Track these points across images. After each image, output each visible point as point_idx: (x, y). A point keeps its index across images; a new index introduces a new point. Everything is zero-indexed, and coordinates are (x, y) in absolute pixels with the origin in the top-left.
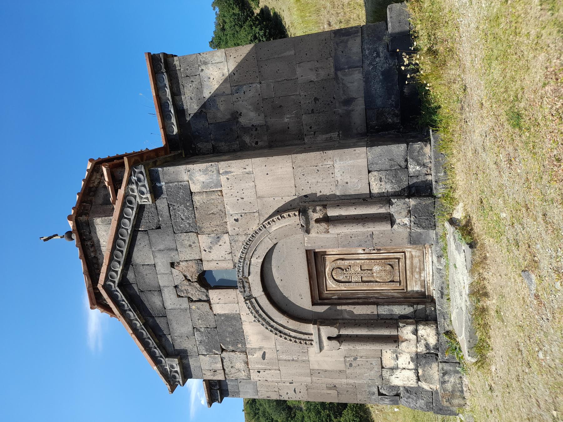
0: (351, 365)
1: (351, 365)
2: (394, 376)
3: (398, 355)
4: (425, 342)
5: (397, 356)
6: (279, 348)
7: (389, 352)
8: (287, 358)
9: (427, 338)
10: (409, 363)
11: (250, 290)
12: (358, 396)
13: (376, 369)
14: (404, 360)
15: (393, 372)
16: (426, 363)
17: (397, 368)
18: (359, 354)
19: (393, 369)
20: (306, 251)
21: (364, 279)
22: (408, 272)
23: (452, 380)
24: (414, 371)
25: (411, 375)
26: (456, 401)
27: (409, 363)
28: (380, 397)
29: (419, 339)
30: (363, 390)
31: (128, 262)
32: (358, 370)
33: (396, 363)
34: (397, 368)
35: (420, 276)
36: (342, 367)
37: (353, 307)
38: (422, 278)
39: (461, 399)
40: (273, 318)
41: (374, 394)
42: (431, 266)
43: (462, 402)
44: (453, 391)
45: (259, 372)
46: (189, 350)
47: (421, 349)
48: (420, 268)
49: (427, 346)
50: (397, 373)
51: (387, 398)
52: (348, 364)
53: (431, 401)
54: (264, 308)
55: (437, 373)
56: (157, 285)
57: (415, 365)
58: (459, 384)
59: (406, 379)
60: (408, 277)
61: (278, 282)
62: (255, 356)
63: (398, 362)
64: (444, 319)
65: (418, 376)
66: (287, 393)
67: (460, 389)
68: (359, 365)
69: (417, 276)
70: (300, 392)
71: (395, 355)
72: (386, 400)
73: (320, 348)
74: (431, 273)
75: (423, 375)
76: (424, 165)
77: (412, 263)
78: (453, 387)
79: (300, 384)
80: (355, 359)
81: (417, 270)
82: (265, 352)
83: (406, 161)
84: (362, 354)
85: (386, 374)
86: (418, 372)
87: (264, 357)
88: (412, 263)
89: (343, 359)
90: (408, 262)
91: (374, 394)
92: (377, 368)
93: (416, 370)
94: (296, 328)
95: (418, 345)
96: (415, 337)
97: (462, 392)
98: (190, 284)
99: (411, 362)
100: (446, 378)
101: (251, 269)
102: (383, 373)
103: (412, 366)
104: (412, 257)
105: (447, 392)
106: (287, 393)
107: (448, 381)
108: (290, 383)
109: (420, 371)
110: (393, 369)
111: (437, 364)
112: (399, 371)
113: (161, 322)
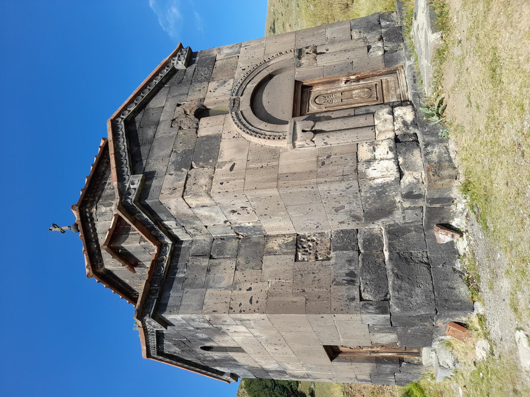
0: (323, 164)
1: (323, 164)
2: (370, 169)
3: (376, 147)
4: (402, 120)
5: (374, 148)
6: (250, 158)
7: (365, 145)
8: (257, 166)
9: (404, 117)
10: (388, 152)
11: (239, 106)
12: (333, 303)
13: (351, 164)
14: (383, 150)
15: (370, 165)
16: (406, 150)
17: (375, 159)
18: (333, 152)
19: (369, 162)
20: (296, 81)
21: (359, 377)
22: (384, 91)
23: (436, 149)
24: (393, 160)
25: (392, 165)
26: (445, 173)
27: (388, 152)
28: (362, 303)
29: (395, 119)
30: (340, 294)
31: (142, 107)
32: (331, 168)
33: (373, 155)
34: (375, 159)
35: (396, 92)
36: (313, 167)
37: (331, 113)
38: (398, 93)
39: (451, 169)
40: (253, 124)
41: (353, 299)
42: (404, 80)
43: (453, 173)
44: (440, 162)
45: (222, 184)
46: (158, 171)
47: (398, 126)
48: (395, 88)
49: (405, 123)
50: (375, 165)
51: (371, 305)
52: (320, 163)
53: (431, 289)
54: (247, 118)
55: (420, 158)
56: (157, 120)
57: (394, 154)
58: (445, 153)
59: (385, 170)
60: (384, 94)
61: (265, 104)
62: (224, 168)
63: (375, 153)
64: (419, 98)
65: (398, 165)
66: (241, 304)
67: (448, 158)
68: (332, 163)
69: (393, 93)
70: (257, 302)
71: (371, 147)
72: (371, 307)
73: (293, 139)
74: (405, 84)
75: (405, 163)
76: (392, 21)
77: (388, 86)
78: (439, 157)
79: (259, 290)
80: (329, 157)
81: (393, 89)
82: (234, 164)
83: (379, 21)
84: (336, 151)
85: (361, 167)
86: (398, 162)
87: (231, 169)
88: (388, 86)
89: (315, 159)
90: (384, 85)
91: (353, 299)
92: (351, 163)
93: (396, 159)
94: (273, 130)
95: (395, 123)
96: (391, 116)
97: (450, 161)
98: (186, 117)
99: (390, 152)
100: (429, 149)
101: (245, 91)
102: (359, 167)
103: (391, 155)
104: (387, 82)
105: (433, 164)
106: (241, 304)
107: (432, 152)
108: (247, 290)
109: (401, 160)
110: (369, 162)
111: (419, 150)
112: (377, 162)
113: (144, 150)
